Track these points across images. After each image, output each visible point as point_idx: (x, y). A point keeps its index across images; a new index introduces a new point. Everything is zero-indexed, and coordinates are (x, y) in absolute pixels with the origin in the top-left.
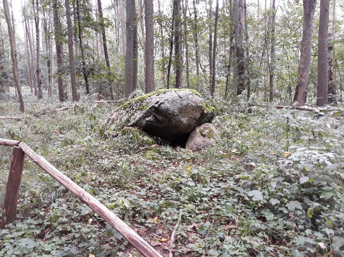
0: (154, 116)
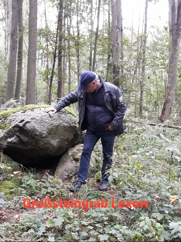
0: (18, 136)
